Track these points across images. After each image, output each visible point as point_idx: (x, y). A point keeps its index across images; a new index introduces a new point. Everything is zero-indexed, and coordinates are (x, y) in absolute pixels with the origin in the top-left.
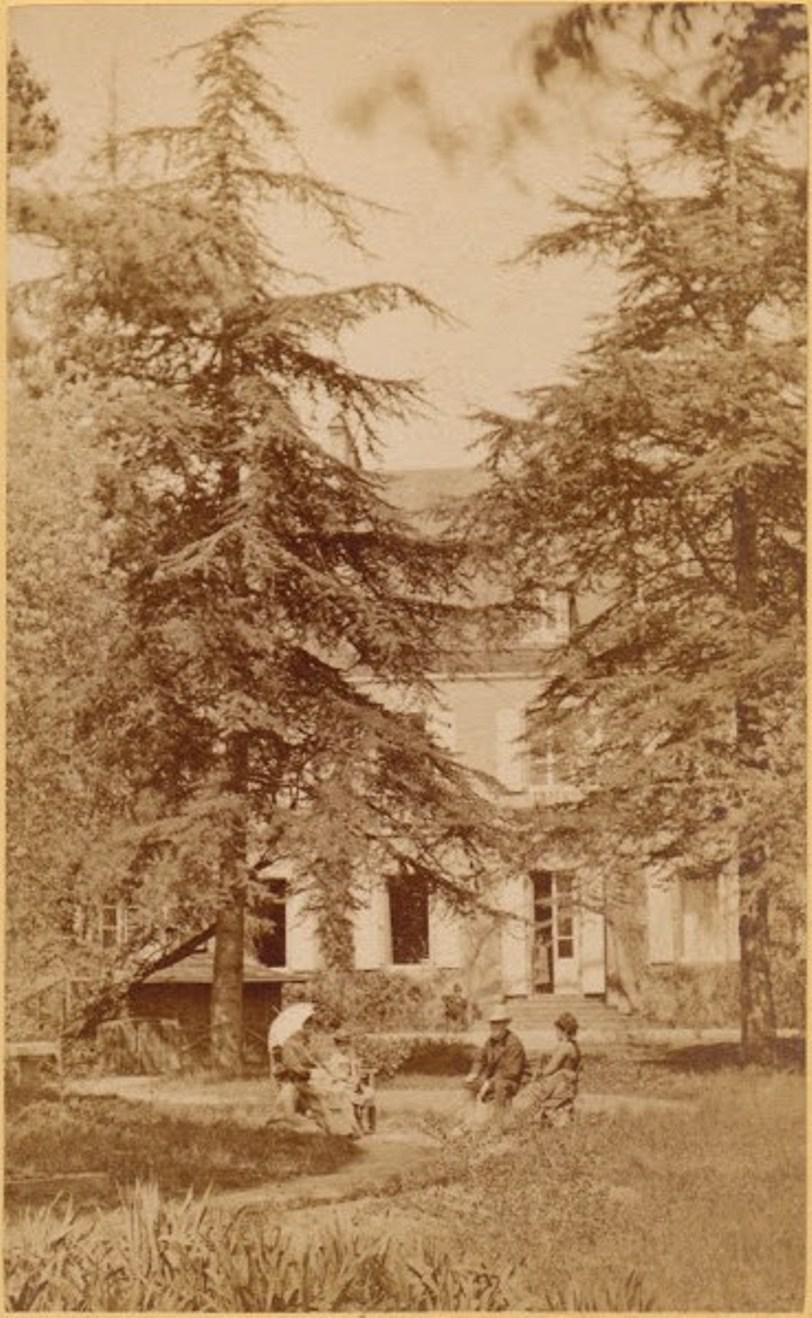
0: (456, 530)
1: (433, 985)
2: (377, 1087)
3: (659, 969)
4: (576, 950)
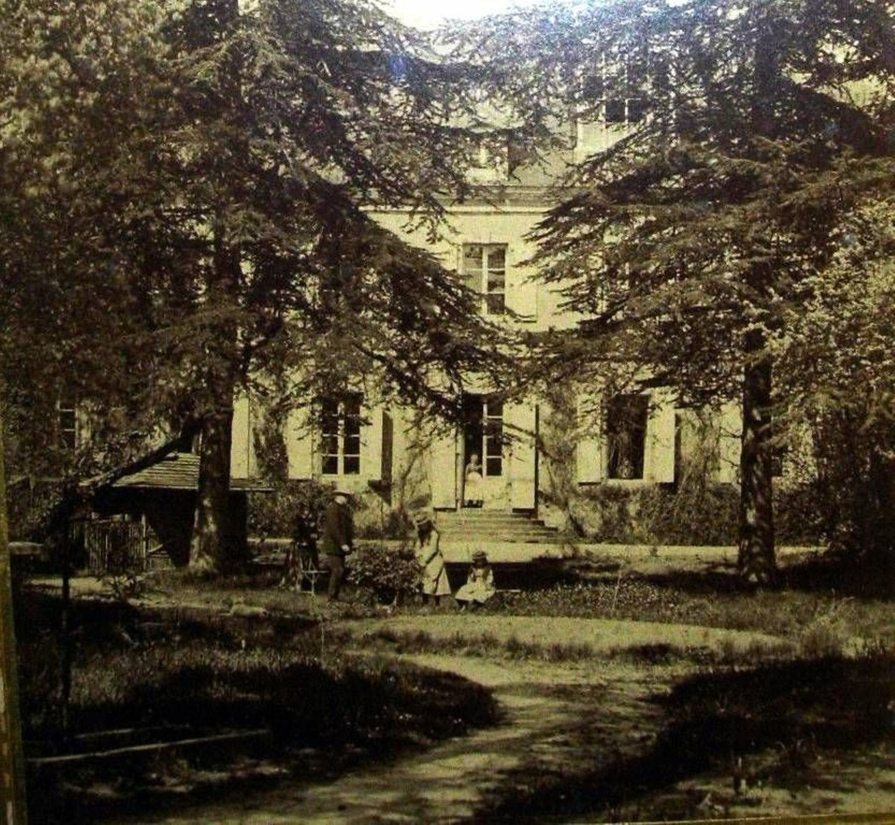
0: (459, 55)
1: (364, 496)
2: (317, 592)
3: (586, 488)
4: (504, 471)
